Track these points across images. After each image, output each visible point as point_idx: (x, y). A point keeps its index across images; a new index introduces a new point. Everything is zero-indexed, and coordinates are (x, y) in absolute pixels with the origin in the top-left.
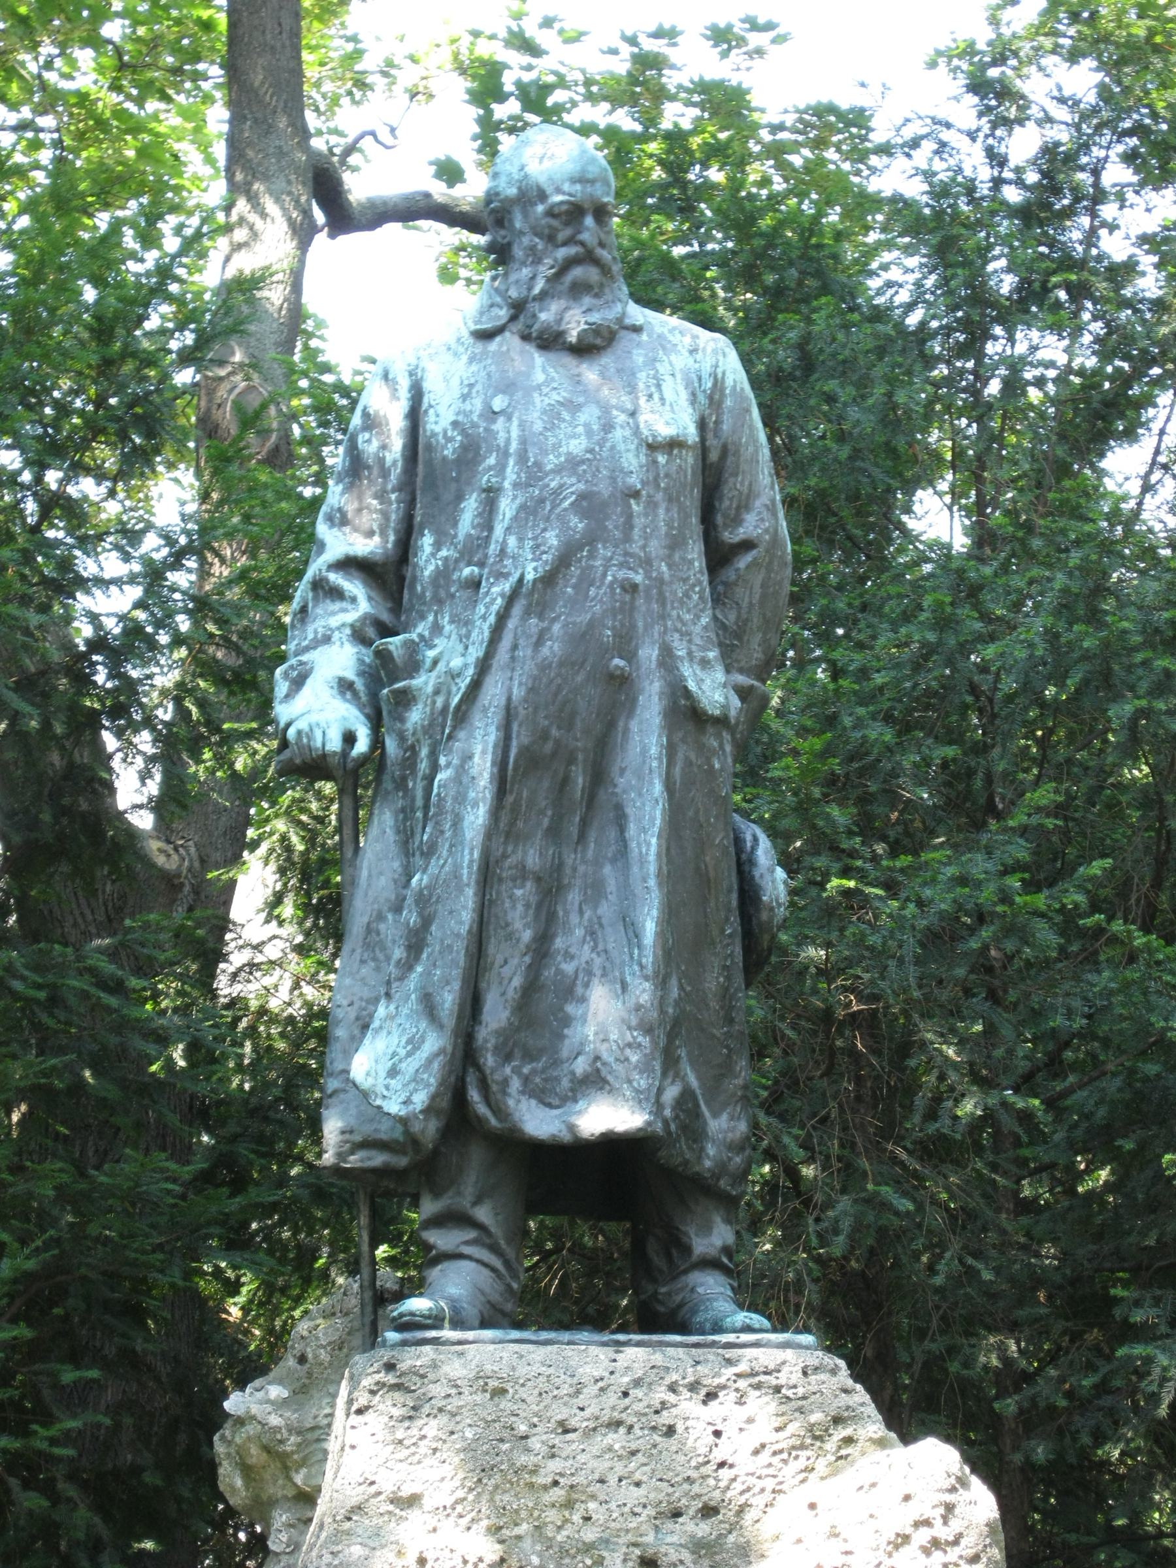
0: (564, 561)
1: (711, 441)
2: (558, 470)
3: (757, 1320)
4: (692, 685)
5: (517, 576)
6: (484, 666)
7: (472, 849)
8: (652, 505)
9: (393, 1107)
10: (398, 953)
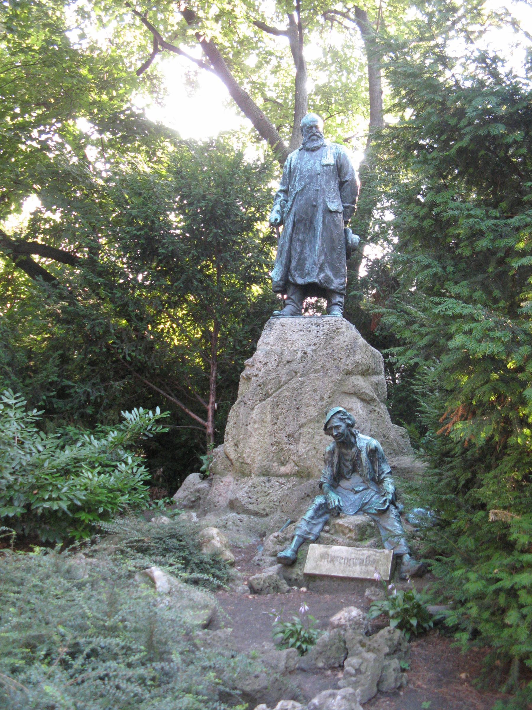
0: (305, 187)
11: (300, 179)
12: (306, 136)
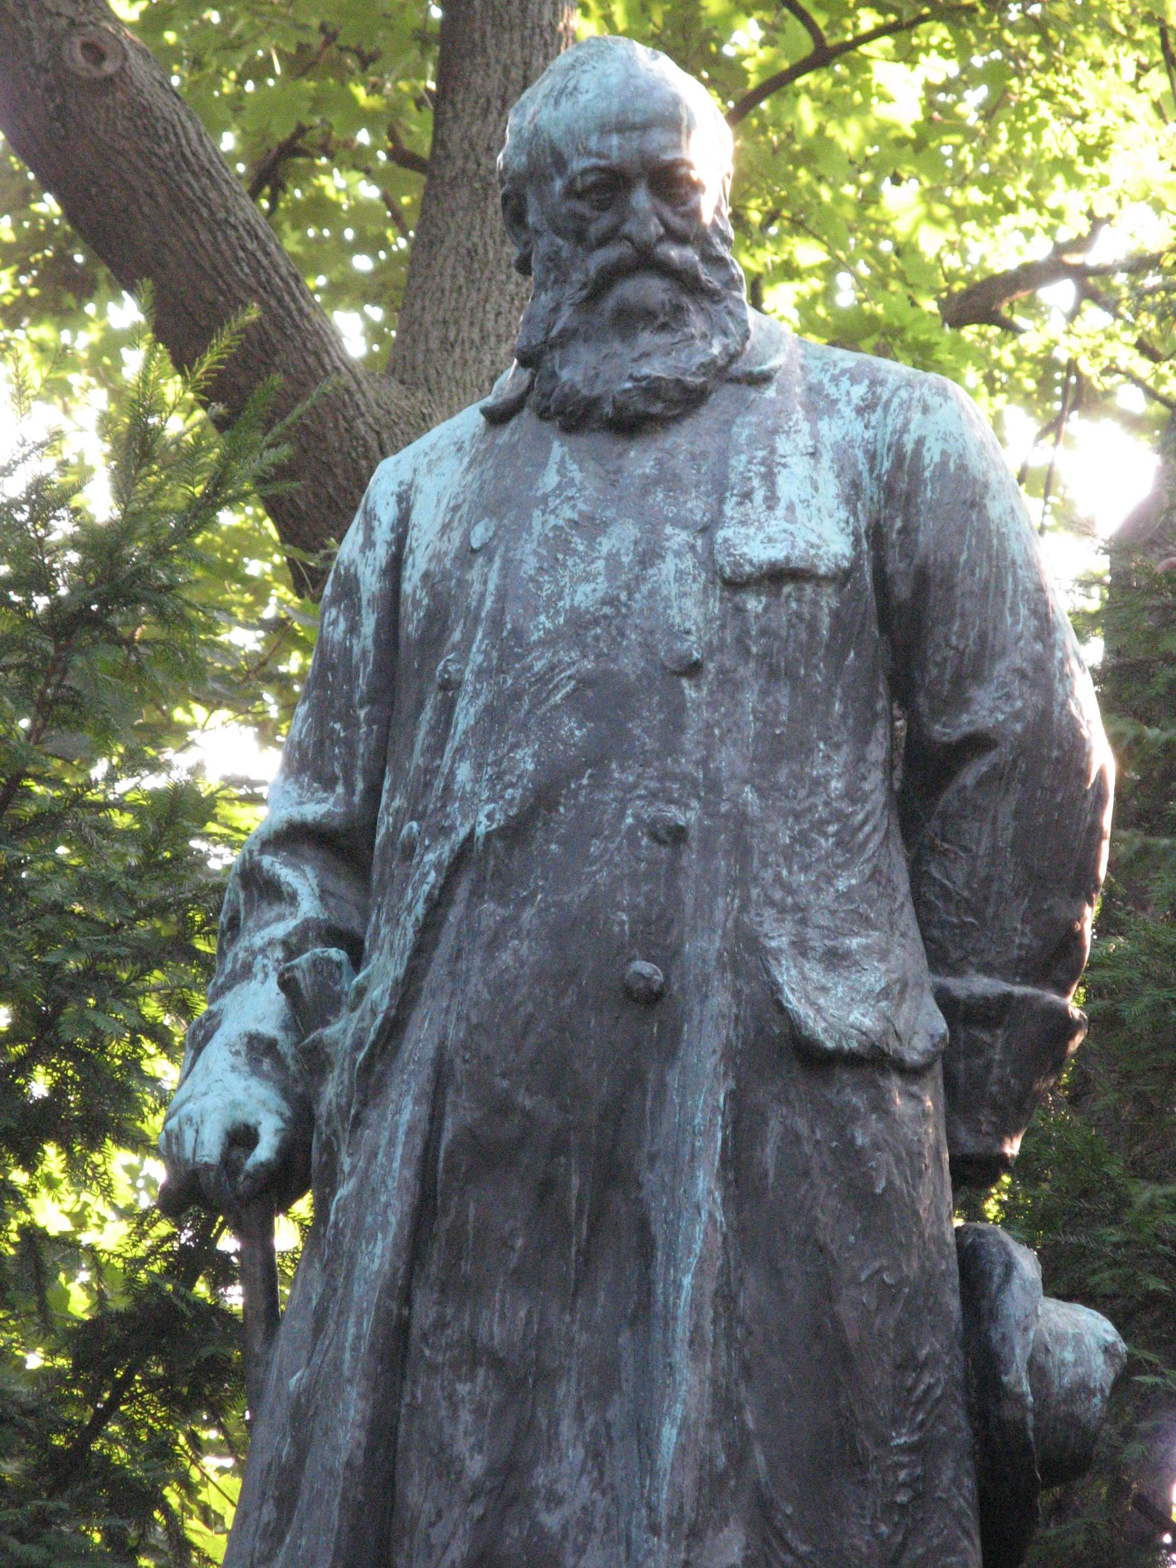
1: (895, 564)
2: (551, 640)
4: (793, 1001)
5: (463, 832)
7: (360, 1319)
11: (493, 716)
12: (557, 268)
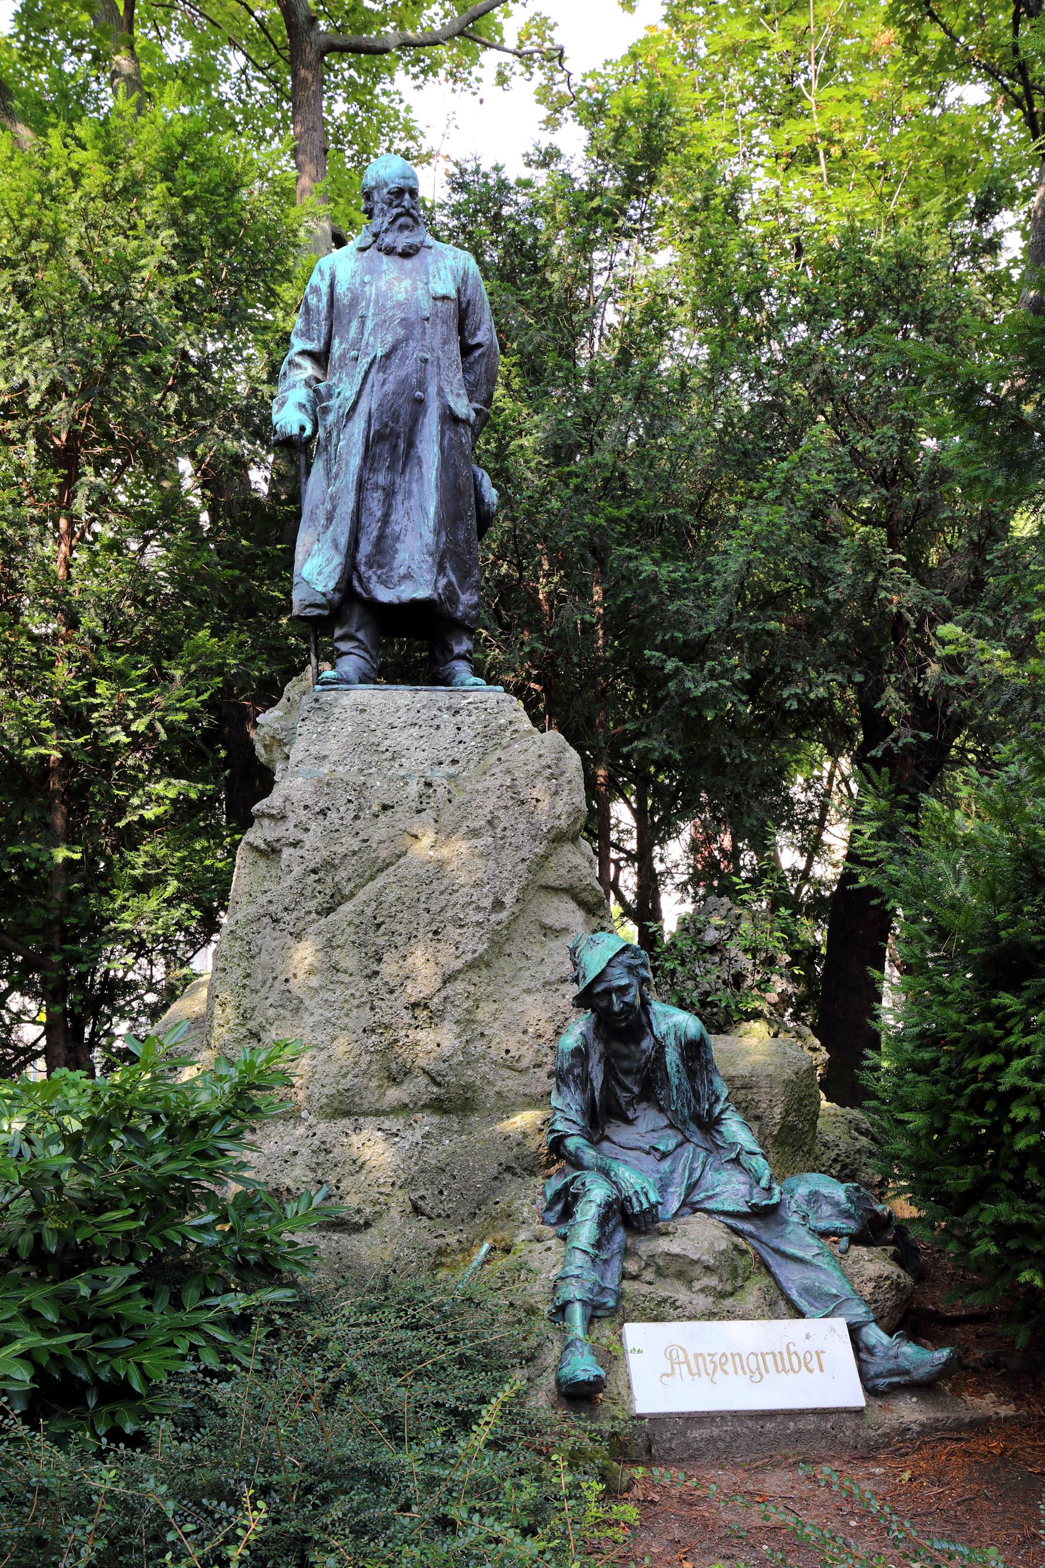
0: (394, 349)
1: (464, 299)
3: (480, 680)
6: (359, 394)
8: (434, 324)
9: (320, 588)
10: (323, 522)
